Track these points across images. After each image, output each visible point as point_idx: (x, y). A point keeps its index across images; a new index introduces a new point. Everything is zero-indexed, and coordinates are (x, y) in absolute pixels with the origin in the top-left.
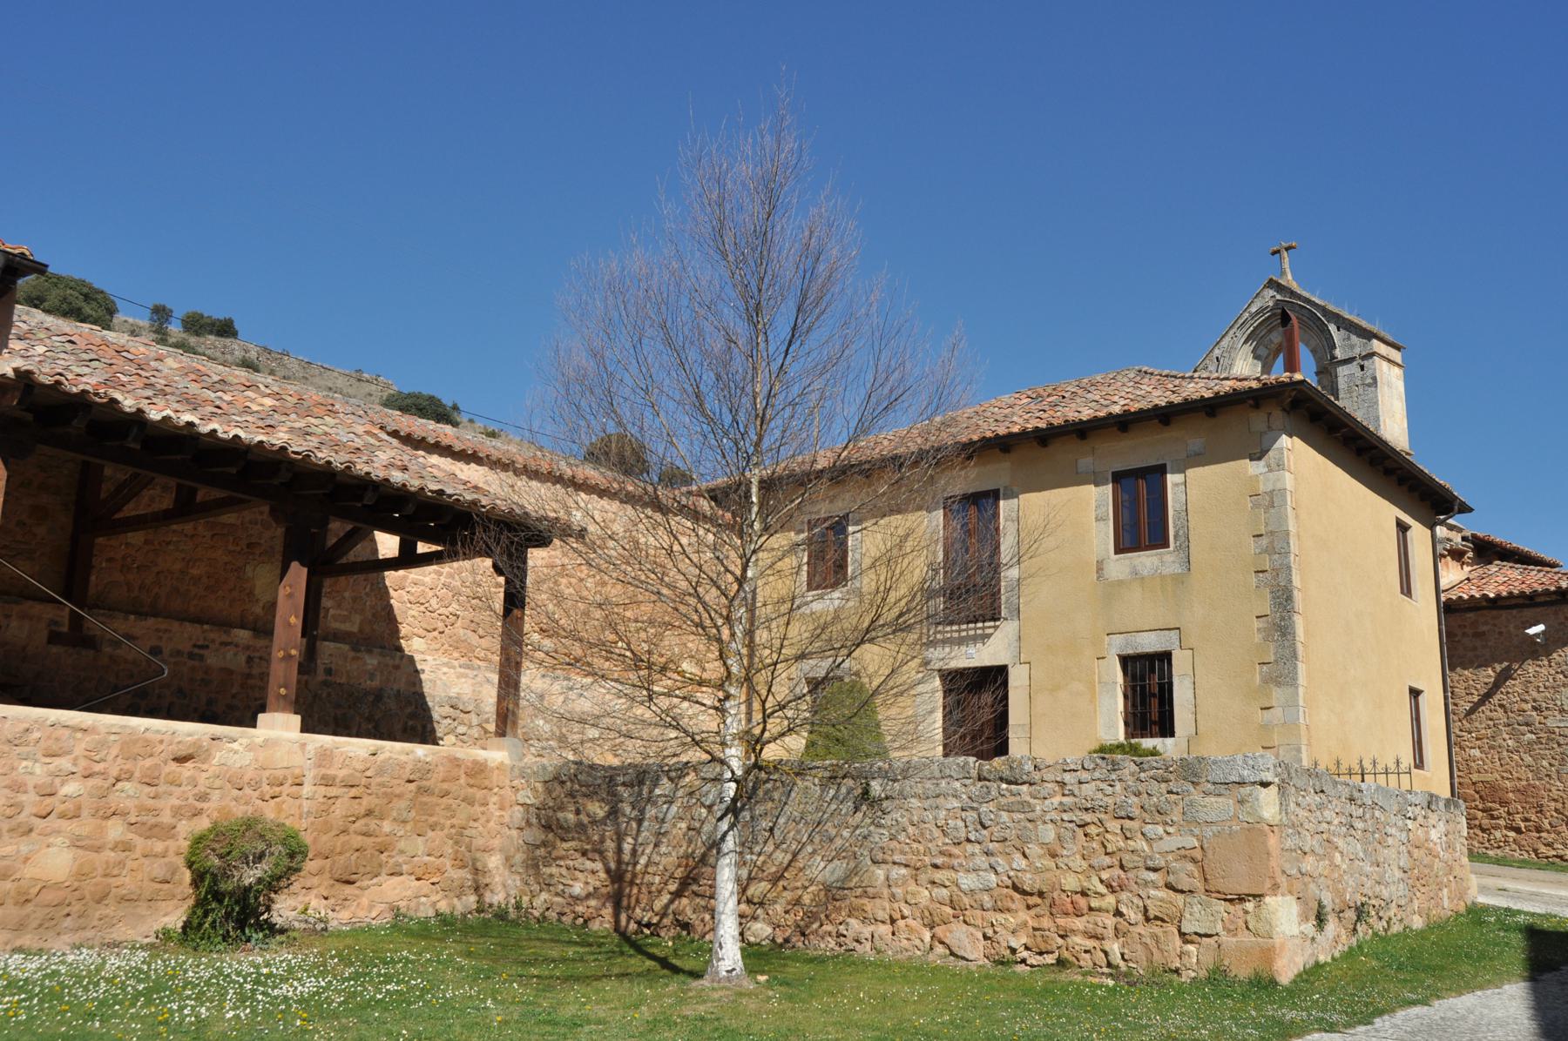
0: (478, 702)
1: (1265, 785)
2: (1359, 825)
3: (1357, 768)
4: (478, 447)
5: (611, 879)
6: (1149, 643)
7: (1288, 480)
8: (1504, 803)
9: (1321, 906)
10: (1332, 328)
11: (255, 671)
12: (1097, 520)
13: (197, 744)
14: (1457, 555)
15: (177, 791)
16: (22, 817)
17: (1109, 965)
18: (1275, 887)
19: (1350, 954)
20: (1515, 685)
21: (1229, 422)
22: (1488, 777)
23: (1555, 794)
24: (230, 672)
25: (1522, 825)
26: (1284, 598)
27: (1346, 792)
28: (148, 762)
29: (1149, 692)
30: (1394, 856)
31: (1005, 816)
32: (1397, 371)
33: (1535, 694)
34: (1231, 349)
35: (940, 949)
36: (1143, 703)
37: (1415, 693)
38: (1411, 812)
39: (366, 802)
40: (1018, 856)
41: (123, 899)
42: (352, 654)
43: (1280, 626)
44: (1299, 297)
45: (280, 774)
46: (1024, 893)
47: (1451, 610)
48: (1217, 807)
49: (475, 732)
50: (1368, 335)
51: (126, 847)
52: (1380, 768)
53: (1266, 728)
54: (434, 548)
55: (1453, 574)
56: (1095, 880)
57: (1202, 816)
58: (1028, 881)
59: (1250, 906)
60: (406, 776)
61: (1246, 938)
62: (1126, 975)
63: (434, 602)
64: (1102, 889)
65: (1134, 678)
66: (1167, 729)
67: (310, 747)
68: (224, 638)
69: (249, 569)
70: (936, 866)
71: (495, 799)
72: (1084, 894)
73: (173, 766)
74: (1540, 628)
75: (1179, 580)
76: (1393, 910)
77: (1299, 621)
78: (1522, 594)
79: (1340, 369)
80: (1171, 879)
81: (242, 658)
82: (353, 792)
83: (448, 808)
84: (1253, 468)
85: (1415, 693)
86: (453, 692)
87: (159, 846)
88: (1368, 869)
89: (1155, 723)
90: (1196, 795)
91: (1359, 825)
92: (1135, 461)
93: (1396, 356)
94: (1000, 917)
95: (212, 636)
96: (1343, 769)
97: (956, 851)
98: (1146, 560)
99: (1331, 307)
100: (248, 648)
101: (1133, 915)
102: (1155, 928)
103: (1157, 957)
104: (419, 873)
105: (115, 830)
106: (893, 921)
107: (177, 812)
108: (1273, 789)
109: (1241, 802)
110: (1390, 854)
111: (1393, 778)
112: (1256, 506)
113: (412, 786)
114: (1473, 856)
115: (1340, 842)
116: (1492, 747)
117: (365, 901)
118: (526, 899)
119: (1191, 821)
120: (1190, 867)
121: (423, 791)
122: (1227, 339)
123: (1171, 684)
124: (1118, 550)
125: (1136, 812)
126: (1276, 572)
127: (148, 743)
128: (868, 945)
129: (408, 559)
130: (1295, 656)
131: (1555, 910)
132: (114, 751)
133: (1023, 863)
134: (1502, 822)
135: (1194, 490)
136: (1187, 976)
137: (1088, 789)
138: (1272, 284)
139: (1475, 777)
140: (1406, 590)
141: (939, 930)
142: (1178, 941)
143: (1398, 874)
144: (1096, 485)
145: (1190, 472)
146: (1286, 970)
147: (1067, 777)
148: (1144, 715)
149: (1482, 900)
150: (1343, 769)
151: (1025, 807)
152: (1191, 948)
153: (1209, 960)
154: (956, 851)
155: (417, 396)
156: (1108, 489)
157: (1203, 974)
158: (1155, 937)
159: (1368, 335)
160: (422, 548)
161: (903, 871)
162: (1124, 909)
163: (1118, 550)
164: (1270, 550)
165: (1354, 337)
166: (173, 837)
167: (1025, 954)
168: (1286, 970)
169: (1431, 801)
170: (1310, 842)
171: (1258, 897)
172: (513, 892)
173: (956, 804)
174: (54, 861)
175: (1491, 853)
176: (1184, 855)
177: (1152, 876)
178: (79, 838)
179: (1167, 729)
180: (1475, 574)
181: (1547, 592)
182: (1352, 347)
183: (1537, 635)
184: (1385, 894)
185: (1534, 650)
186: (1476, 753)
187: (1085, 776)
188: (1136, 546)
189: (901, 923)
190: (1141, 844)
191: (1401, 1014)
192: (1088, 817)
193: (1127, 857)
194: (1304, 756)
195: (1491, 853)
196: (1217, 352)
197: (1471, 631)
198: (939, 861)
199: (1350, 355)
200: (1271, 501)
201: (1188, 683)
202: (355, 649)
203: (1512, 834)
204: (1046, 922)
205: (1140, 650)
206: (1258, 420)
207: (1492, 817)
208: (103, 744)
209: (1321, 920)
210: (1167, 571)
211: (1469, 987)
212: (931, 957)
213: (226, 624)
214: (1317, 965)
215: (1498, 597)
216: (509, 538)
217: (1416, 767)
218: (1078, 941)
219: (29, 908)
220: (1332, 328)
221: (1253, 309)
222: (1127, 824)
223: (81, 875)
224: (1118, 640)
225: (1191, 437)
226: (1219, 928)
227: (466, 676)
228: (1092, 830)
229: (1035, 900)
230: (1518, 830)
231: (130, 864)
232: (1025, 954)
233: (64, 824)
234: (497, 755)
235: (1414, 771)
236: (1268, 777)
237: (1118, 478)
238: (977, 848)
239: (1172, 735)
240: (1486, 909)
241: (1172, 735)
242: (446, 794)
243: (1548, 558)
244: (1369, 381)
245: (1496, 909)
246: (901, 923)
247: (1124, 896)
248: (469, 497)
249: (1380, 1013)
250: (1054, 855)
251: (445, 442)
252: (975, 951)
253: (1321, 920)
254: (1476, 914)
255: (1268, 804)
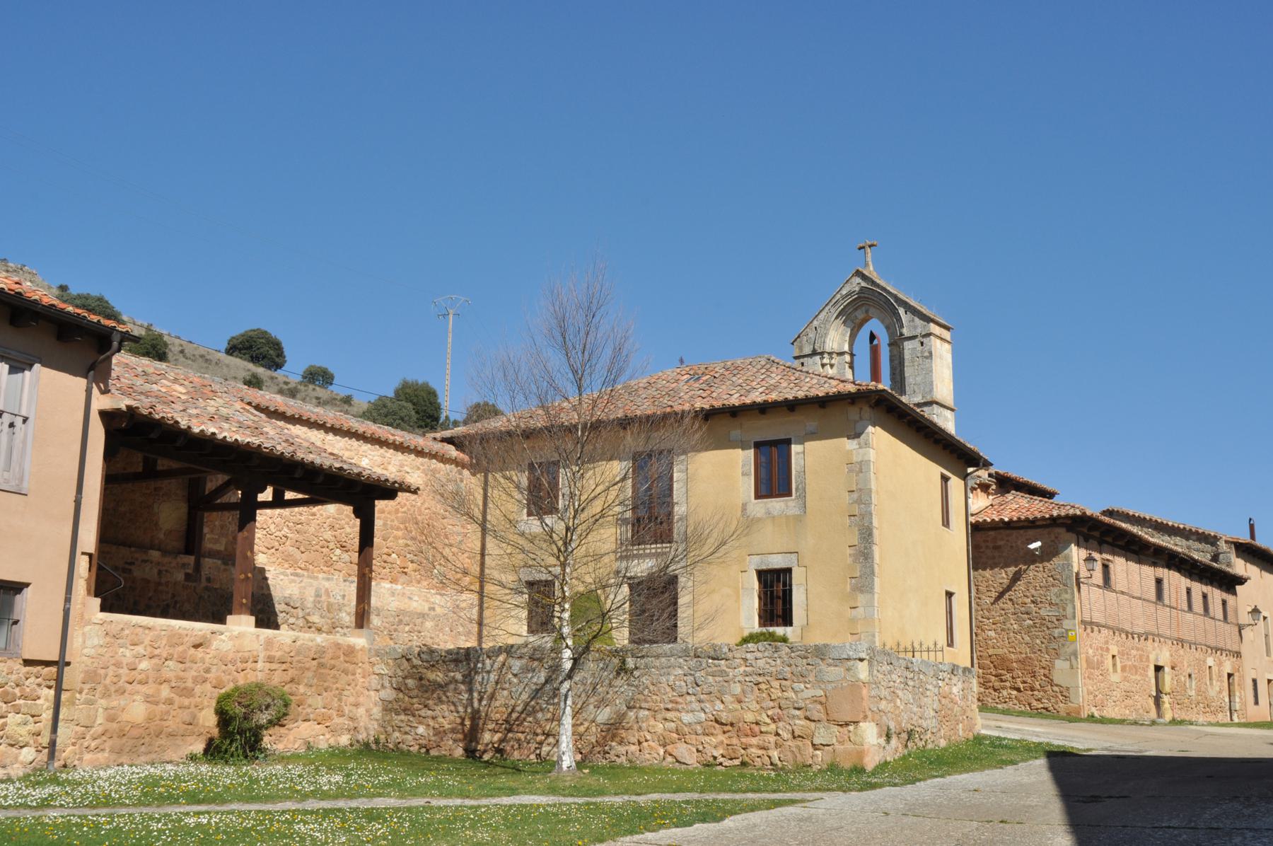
0: (302, 600)
1: (861, 660)
2: (911, 683)
3: (910, 648)
4: (302, 412)
5: (463, 716)
6: (777, 562)
7: (872, 455)
8: (1010, 670)
9: (889, 729)
10: (901, 311)
11: (163, 580)
12: (743, 474)
13: (204, 637)
14: (984, 488)
15: (195, 666)
16: (121, 683)
17: (772, 764)
18: (865, 717)
19: (904, 758)
20: (1021, 585)
21: (835, 412)
22: (1000, 651)
23: (1044, 663)
24: (148, 581)
25: (1021, 686)
26: (867, 535)
27: (903, 663)
28: (181, 649)
29: (776, 595)
30: (931, 702)
31: (710, 678)
32: (947, 347)
33: (1033, 592)
34: (826, 321)
35: (670, 759)
36: (772, 603)
37: (949, 595)
38: (941, 675)
39: (291, 673)
40: (718, 702)
41: (170, 735)
42: (223, 567)
43: (864, 554)
44: (878, 286)
45: (246, 654)
46: (722, 724)
47: (977, 530)
48: (834, 673)
49: (301, 622)
50: (928, 320)
51: (170, 702)
52: (924, 647)
53: (853, 621)
54: (300, 496)
55: (980, 502)
56: (764, 716)
57: (826, 678)
58: (724, 717)
59: (851, 728)
60: (312, 655)
61: (849, 746)
62: (782, 769)
63: (272, 527)
64: (768, 721)
65: (765, 586)
66: (787, 620)
67: (262, 638)
68: (145, 557)
69: (155, 506)
70: (667, 709)
71: (359, 671)
72: (757, 723)
73: (193, 650)
74: (1038, 544)
75: (798, 519)
76: (929, 735)
77: (876, 550)
78: (1027, 519)
79: (906, 343)
80: (808, 714)
81: (155, 571)
82: (284, 667)
83: (334, 677)
84: (850, 445)
85: (949, 595)
86: (287, 593)
87: (186, 702)
88: (915, 709)
89: (778, 616)
90: (823, 666)
91: (911, 683)
92: (770, 433)
93: (946, 335)
94: (707, 739)
95: (137, 555)
96: (901, 648)
97: (680, 700)
98: (776, 505)
99: (901, 296)
100: (158, 563)
101: (785, 735)
102: (798, 742)
103: (799, 758)
104: (320, 719)
105: (165, 692)
106: (640, 743)
107: (195, 680)
108: (866, 662)
109: (848, 670)
110: (928, 701)
111: (932, 654)
112: (850, 471)
113: (315, 663)
114: (984, 708)
115: (900, 693)
116: (1003, 630)
117: (291, 738)
118: (382, 737)
119: (820, 681)
120: (819, 707)
121: (321, 665)
122: (824, 313)
123: (791, 591)
124: (757, 497)
125: (789, 676)
126: (863, 516)
127: (180, 636)
128: (623, 758)
129: (279, 502)
130: (873, 573)
131: (1026, 737)
132: (164, 642)
133: (722, 706)
134: (1008, 684)
135: (811, 457)
136: (816, 768)
137: (761, 663)
138: (858, 274)
139: (991, 651)
140: (946, 523)
141: (669, 748)
142: (811, 749)
143: (932, 713)
144: (743, 449)
145: (807, 444)
146: (870, 763)
147: (749, 656)
148: (772, 611)
149: (984, 732)
150: (901, 648)
151: (723, 673)
152: (818, 752)
153: (828, 759)
154: (680, 700)
155: (87, 297)
156: (751, 453)
157: (825, 766)
158: (798, 747)
159: (928, 320)
160: (289, 495)
161: (646, 713)
162: (780, 732)
163: (757, 497)
164: (859, 501)
165: (916, 319)
166: (193, 696)
167: (722, 760)
168: (870, 763)
169: (954, 670)
170: (884, 693)
171: (856, 723)
172: (372, 733)
173: (680, 672)
174: (136, 711)
175: (1000, 706)
176: (815, 700)
177: (797, 712)
178: (148, 696)
179: (787, 620)
180: (997, 501)
181: (1043, 518)
182: (915, 327)
183: (1036, 549)
184: (925, 725)
185: (1032, 558)
186: (992, 634)
187: (759, 655)
188: (770, 495)
189: (645, 744)
190: (791, 694)
191: (929, 781)
192: (761, 679)
193: (783, 702)
194: (877, 639)
195: (1000, 706)
196: (815, 323)
197: (990, 544)
198: (670, 706)
199: (914, 334)
200: (860, 468)
201: (802, 589)
202: (225, 563)
203: (1015, 692)
204: (735, 741)
205: (770, 567)
206: (853, 412)
207: (1002, 681)
208: (159, 637)
209: (888, 737)
210: (790, 512)
211: (967, 771)
212: (664, 764)
213: (144, 547)
214: (886, 763)
215: (1011, 521)
216: (362, 494)
217: (949, 645)
218: (754, 751)
219: (125, 739)
220: (901, 311)
221: (844, 292)
222: (784, 682)
223: (150, 719)
224: (756, 559)
225: (811, 421)
226: (834, 741)
227: (294, 581)
228: (763, 686)
229: (729, 728)
230: (1018, 690)
231: (173, 713)
232: (722, 760)
233: (139, 687)
234: (359, 641)
235: (946, 649)
236: (863, 655)
237: (758, 445)
238: (693, 698)
239: (791, 625)
240: (985, 737)
241: (791, 625)
242: (333, 668)
243: (1049, 487)
244: (926, 354)
245: (990, 737)
246: (645, 744)
247: (781, 724)
248: (337, 465)
249: (920, 780)
250: (740, 702)
251: (281, 409)
252: (692, 759)
253: (888, 737)
254: (979, 739)
255: (863, 671)
